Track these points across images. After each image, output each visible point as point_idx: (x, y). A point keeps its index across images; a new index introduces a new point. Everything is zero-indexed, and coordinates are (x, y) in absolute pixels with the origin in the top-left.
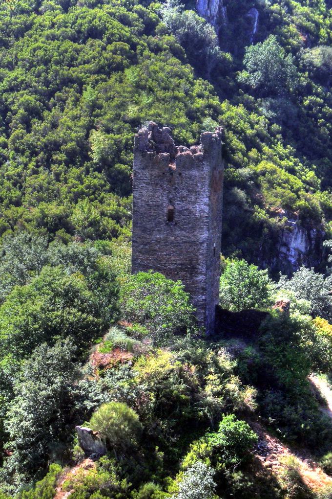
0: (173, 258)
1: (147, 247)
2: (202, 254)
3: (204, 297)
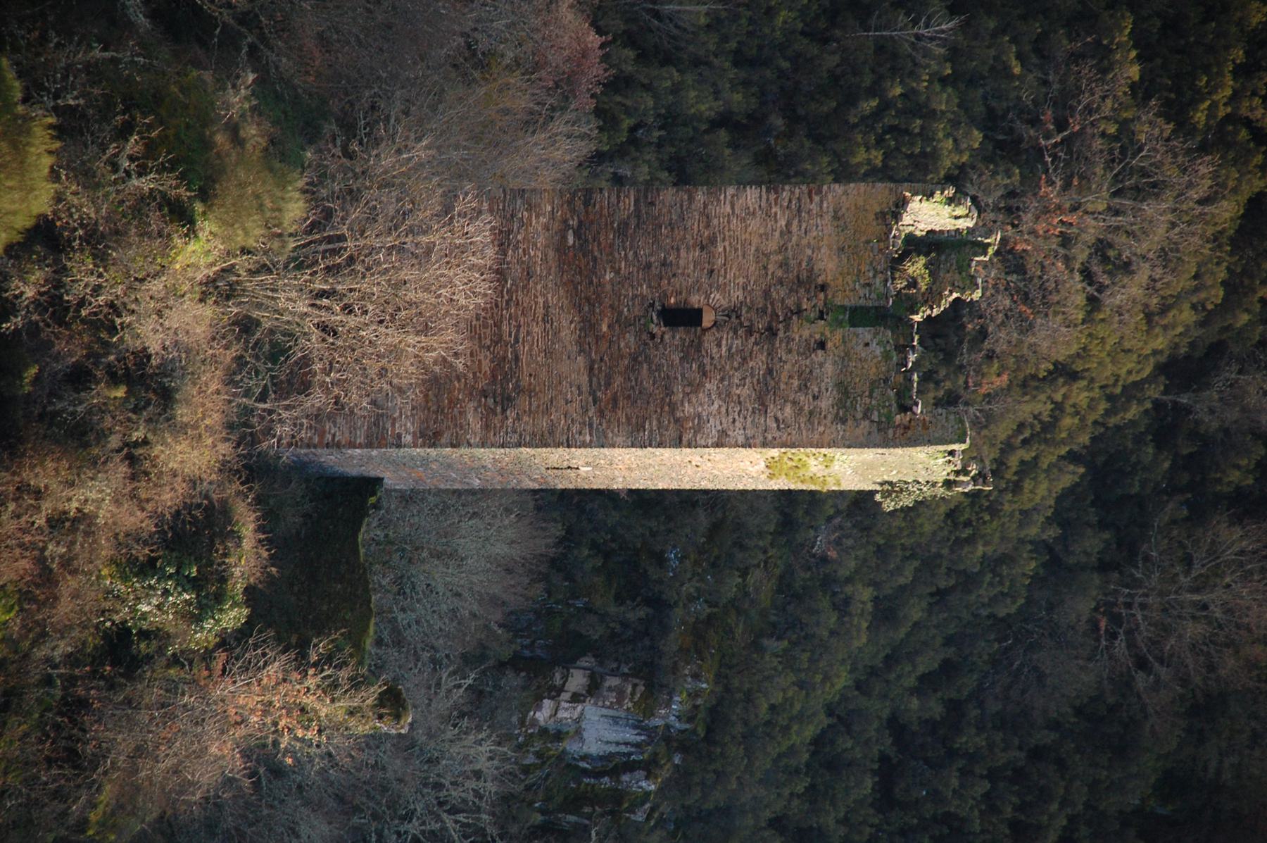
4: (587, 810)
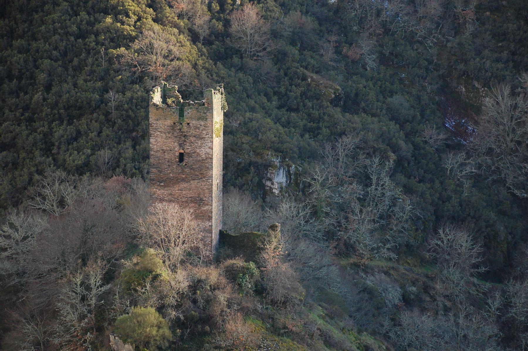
4: (299, 181)
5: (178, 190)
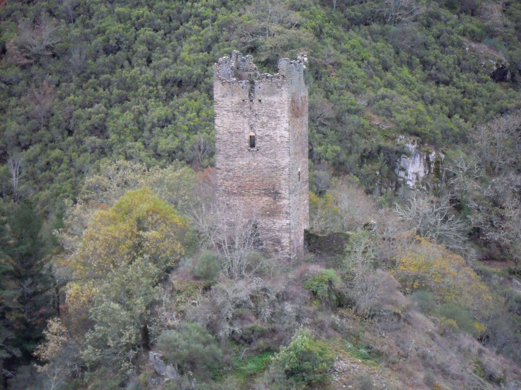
0: (256, 184)
1: (230, 174)
2: (285, 179)
3: (288, 222)
4: (441, 171)
5: (249, 181)
